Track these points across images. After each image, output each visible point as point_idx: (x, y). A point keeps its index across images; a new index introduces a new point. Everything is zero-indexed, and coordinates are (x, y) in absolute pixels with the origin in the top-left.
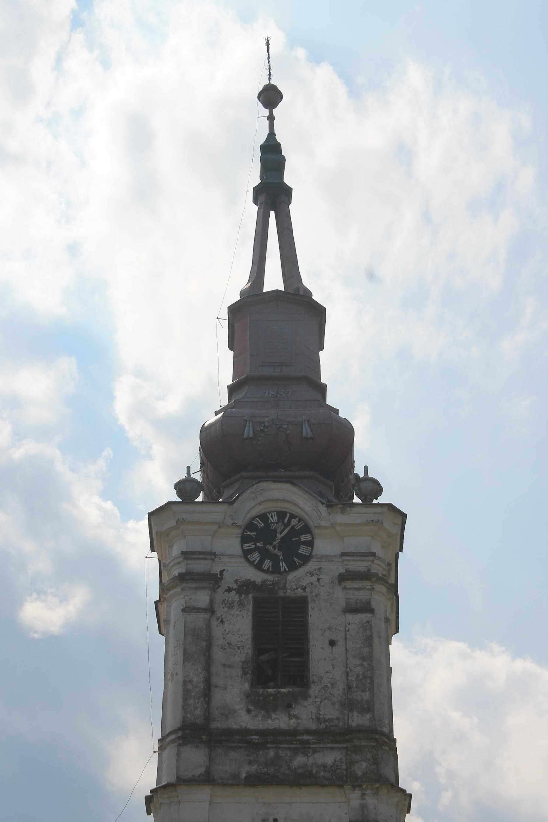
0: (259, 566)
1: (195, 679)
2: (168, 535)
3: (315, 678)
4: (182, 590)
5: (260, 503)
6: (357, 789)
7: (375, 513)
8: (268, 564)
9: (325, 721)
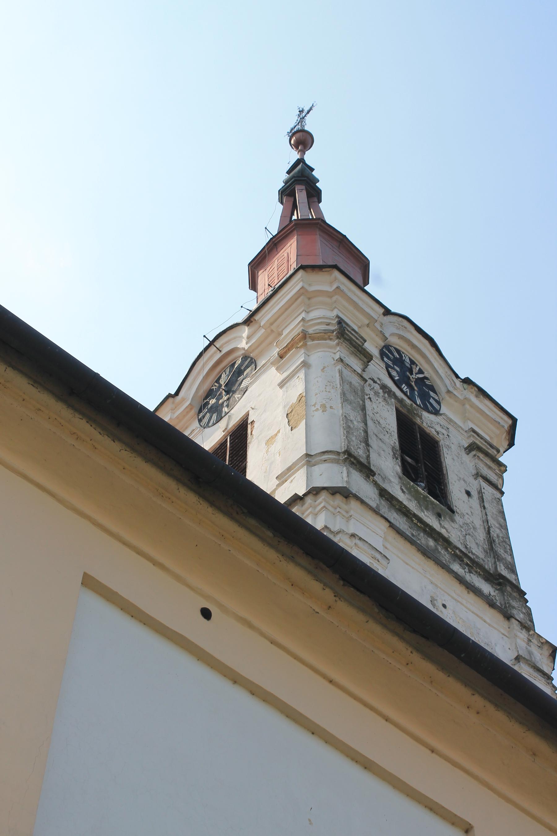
0: (398, 384)
1: (355, 423)
2: (309, 299)
3: (458, 511)
4: (338, 344)
5: (401, 337)
6: (524, 630)
7: (502, 418)
8: (404, 387)
9: (472, 553)
